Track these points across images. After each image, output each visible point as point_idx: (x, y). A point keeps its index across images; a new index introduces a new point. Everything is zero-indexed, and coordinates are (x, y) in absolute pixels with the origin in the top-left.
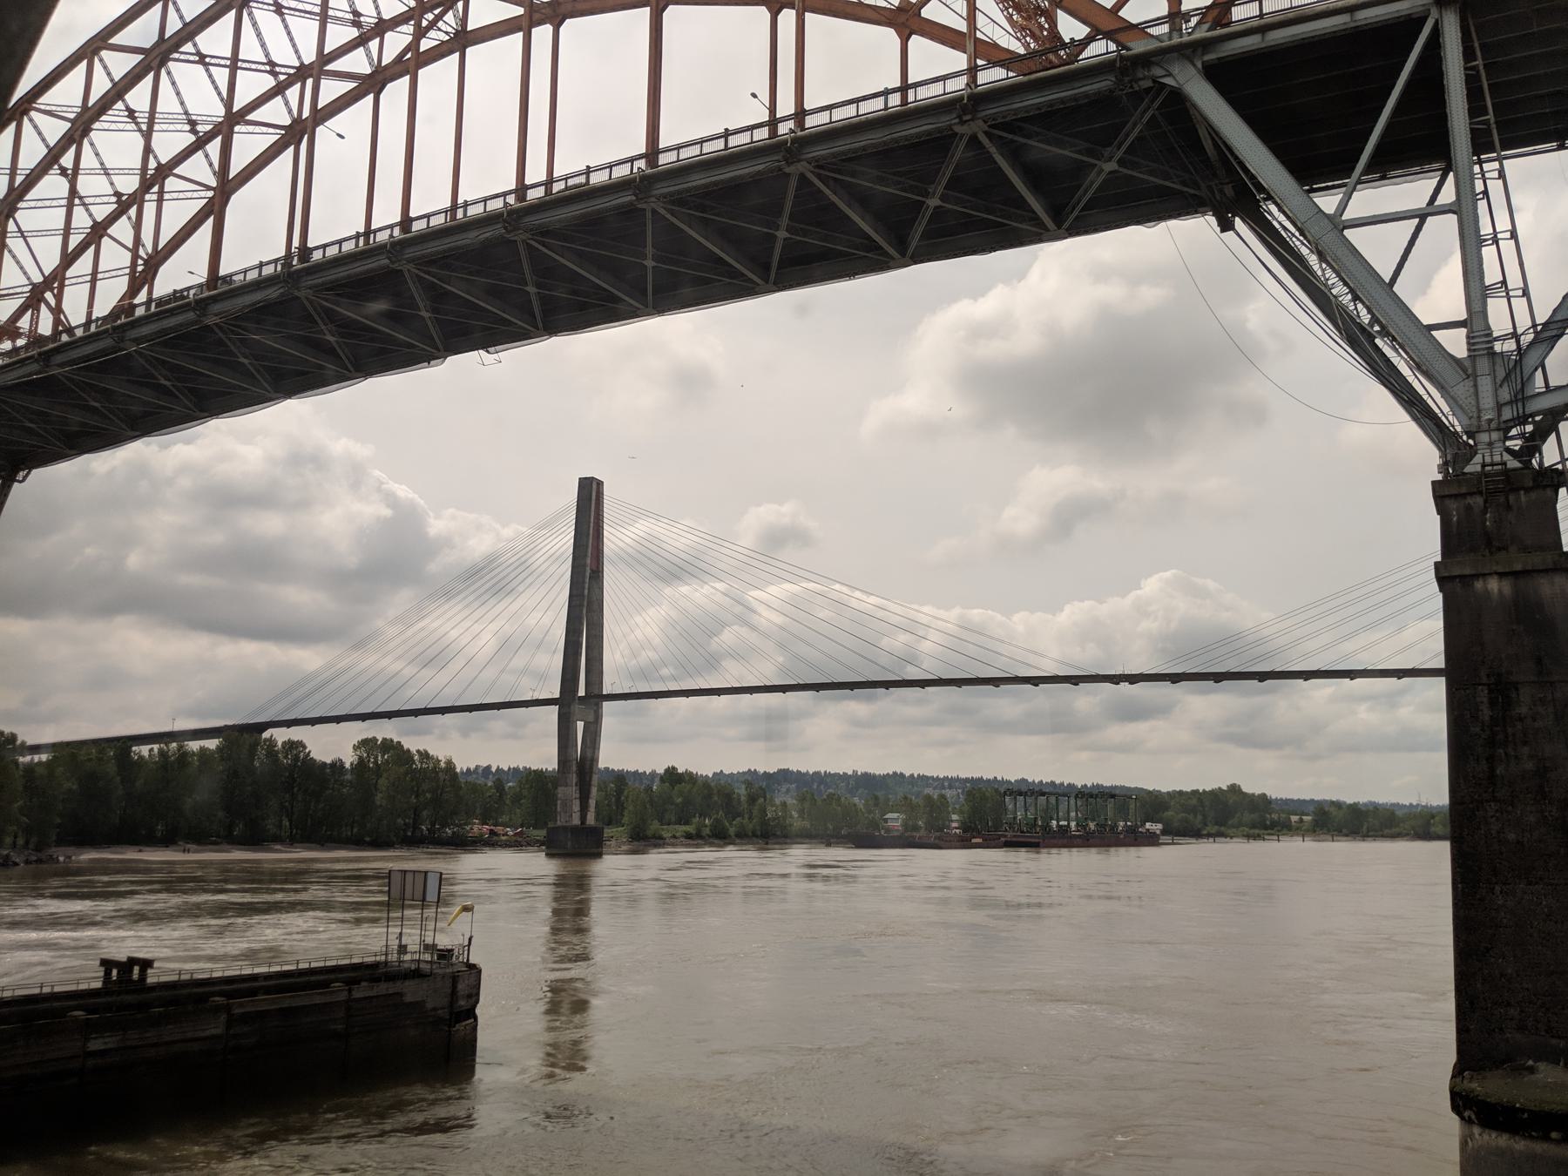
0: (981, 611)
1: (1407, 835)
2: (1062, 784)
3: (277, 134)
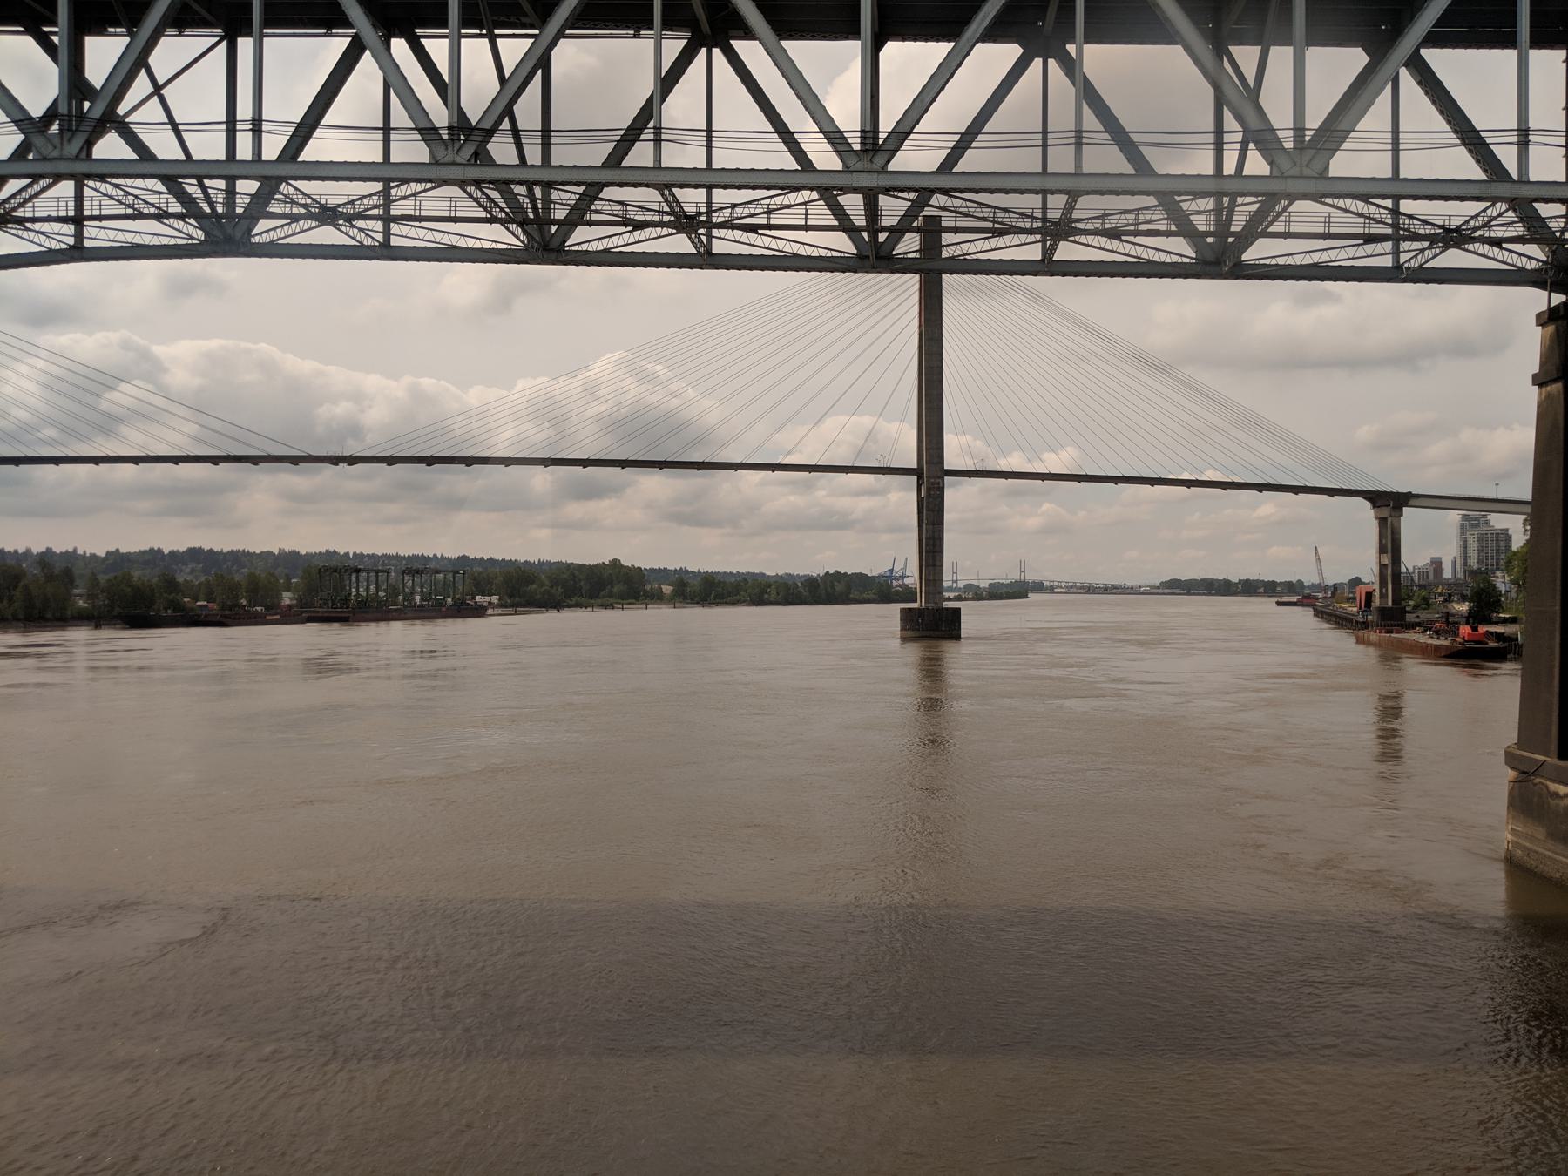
0: (434, 381)
1: (744, 602)
2: (347, 554)
3: (941, 148)
